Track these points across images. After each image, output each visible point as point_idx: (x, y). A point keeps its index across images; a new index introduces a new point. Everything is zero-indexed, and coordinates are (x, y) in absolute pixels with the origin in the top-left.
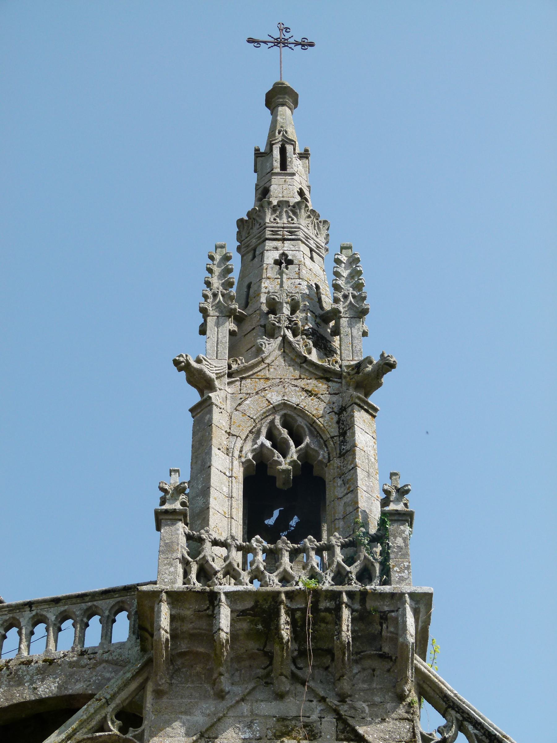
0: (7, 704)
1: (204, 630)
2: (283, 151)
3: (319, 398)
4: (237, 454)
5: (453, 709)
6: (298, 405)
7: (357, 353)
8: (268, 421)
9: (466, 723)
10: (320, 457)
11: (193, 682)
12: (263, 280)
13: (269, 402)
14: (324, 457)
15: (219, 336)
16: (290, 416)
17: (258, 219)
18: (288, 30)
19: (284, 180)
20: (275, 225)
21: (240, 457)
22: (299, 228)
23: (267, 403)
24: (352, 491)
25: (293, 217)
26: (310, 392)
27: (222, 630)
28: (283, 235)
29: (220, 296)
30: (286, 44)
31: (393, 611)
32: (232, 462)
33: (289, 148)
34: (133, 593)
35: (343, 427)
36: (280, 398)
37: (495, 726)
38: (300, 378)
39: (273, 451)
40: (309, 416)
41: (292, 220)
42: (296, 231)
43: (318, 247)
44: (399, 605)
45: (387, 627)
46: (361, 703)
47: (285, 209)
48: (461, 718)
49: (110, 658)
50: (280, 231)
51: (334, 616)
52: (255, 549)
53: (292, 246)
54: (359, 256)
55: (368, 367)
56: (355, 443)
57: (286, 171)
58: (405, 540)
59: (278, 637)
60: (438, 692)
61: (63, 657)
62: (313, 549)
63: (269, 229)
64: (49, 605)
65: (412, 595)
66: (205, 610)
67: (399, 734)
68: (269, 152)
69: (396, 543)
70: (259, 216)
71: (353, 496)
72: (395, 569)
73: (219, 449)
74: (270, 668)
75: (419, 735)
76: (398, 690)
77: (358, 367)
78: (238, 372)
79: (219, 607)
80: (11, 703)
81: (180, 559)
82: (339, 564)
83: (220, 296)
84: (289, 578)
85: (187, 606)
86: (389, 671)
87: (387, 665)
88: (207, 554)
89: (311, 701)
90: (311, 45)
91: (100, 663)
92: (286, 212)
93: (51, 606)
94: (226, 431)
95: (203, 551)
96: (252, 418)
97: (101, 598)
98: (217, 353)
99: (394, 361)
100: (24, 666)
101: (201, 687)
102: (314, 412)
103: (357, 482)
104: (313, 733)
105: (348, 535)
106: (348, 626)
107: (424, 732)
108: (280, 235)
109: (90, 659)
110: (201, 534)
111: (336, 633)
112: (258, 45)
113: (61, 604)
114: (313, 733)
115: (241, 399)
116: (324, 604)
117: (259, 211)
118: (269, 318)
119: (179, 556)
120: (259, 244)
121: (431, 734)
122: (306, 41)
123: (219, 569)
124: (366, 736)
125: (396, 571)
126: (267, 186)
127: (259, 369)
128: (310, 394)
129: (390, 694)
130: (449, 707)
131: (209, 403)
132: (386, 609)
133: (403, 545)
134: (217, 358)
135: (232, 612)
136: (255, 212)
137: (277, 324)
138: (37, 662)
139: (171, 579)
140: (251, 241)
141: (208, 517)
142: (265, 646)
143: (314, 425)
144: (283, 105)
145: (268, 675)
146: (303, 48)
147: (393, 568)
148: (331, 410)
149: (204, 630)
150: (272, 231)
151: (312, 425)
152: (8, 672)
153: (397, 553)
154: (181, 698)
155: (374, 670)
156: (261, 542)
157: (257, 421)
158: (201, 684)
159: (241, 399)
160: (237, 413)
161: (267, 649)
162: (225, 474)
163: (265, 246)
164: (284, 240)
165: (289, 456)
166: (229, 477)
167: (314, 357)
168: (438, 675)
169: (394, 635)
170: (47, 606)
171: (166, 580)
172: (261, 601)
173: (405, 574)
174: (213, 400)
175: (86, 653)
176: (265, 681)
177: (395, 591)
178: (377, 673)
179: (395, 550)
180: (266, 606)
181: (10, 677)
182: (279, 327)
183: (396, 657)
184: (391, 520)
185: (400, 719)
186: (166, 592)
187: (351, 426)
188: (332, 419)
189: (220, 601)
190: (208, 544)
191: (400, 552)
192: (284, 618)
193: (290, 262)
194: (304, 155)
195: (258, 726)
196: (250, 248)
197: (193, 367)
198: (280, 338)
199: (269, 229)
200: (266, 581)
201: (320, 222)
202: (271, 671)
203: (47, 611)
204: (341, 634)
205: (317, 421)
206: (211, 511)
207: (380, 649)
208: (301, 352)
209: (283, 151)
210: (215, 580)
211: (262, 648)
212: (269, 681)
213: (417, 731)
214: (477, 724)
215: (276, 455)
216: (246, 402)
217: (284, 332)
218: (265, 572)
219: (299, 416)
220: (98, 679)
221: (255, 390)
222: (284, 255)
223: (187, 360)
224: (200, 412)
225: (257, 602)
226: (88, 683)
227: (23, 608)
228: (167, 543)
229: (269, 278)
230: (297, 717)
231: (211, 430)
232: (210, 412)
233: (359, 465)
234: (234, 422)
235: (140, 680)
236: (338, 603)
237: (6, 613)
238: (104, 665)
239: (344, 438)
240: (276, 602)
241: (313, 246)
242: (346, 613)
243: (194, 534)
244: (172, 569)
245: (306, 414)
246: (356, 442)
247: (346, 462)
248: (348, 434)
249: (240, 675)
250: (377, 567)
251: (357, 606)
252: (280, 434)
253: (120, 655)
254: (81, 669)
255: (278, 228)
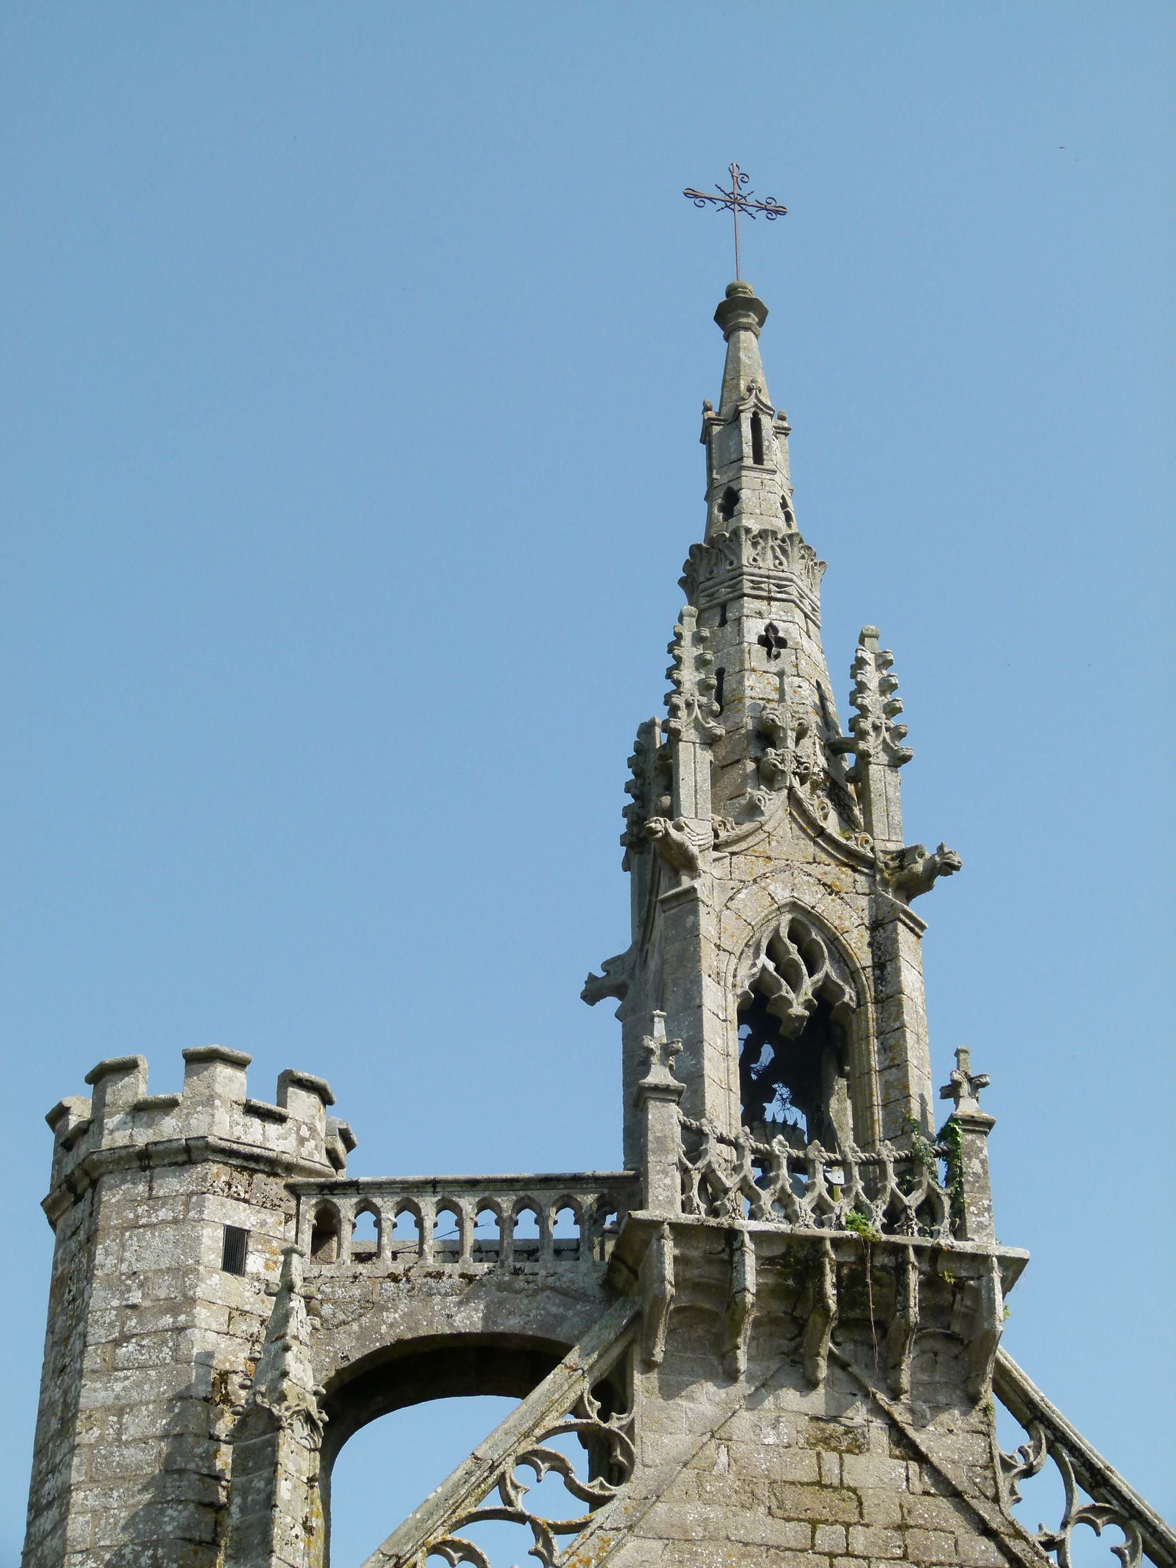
0: (410, 1336)
1: (714, 1279)
2: (756, 424)
3: (842, 899)
4: (730, 980)
5: (1042, 1422)
6: (813, 908)
7: (895, 828)
8: (771, 929)
9: (1059, 1446)
10: (846, 998)
11: (693, 1351)
12: (747, 674)
13: (772, 898)
14: (851, 998)
15: (698, 779)
16: (803, 924)
17: (727, 552)
18: (746, 179)
19: (760, 480)
20: (756, 571)
21: (734, 986)
22: (791, 580)
23: (770, 899)
24: (899, 1065)
25: (781, 557)
26: (829, 887)
27: (749, 1291)
28: (770, 591)
29: (697, 709)
30: (744, 207)
31: (972, 1279)
32: (726, 997)
33: (767, 423)
34: (585, 1186)
35: (879, 953)
36: (787, 894)
37: (1096, 1451)
38: (815, 862)
39: (779, 981)
40: (829, 928)
41: (781, 564)
42: (786, 586)
43: (814, 610)
44: (982, 1271)
45: (962, 1300)
46: (921, 1403)
47: (769, 545)
48: (1052, 1438)
49: (558, 1284)
50: (765, 582)
51: (894, 1278)
52: (778, 1157)
53: (783, 613)
54: (892, 657)
55: (916, 862)
56: (900, 988)
57: (762, 464)
58: (983, 1162)
59: (823, 1307)
60: (1021, 1394)
61: (489, 1274)
62: (856, 1163)
63: (749, 577)
64: (462, 1187)
65: (1001, 1259)
66: (719, 1253)
67: (972, 1454)
68: (730, 420)
69: (972, 1169)
70: (729, 547)
71: (900, 1074)
72: (972, 1209)
73: (710, 976)
74: (798, 1339)
75: (998, 1458)
76: (971, 1389)
77: (902, 855)
78: (727, 844)
79: (743, 1255)
80: (416, 1335)
81: (676, 1164)
82: (892, 1190)
83: (697, 709)
84: (825, 1207)
85: (695, 1243)
86: (956, 1357)
87: (956, 1349)
88: (713, 1159)
89: (855, 1395)
90: (780, 211)
91: (543, 1290)
92: (772, 548)
93: (464, 1189)
94: (715, 944)
95: (707, 1154)
96: (750, 924)
97: (538, 1187)
98: (696, 808)
99: (959, 862)
100: (432, 1280)
101: (705, 1359)
102: (837, 923)
103: (906, 1054)
104: (858, 1443)
105: (892, 1135)
106: (915, 1298)
107: (1004, 1453)
108: (765, 590)
109: (528, 1283)
110: (701, 1125)
111: (899, 1307)
112: (702, 204)
113: (478, 1187)
114: (858, 1443)
115: (733, 889)
116: (883, 1260)
117: (730, 539)
118: (767, 753)
119: (676, 1160)
120: (732, 599)
121: (1011, 1457)
122: (774, 203)
123: (732, 1186)
124: (930, 1455)
125: (973, 1213)
126: (736, 488)
127: (757, 840)
128: (829, 890)
129: (958, 1392)
130: (1036, 1418)
131: (692, 897)
132: (964, 1274)
133: (980, 1171)
134: (696, 817)
135: (757, 1258)
136: (723, 539)
137: (780, 766)
138: (450, 1276)
139: (668, 1197)
140: (717, 588)
141: (703, 1090)
142: (794, 1309)
143: (836, 943)
144: (747, 328)
145: (796, 1350)
146: (769, 216)
147: (968, 1208)
148: (860, 922)
149: (714, 1279)
150: (752, 581)
151: (832, 943)
152: (408, 1286)
153: (973, 1184)
154: (680, 1374)
155: (936, 1354)
156: (784, 1146)
157: (756, 928)
158: (705, 1354)
159: (733, 889)
160: (727, 912)
161: (797, 1313)
162: (717, 1016)
163: (742, 607)
164: (770, 599)
165: (803, 991)
166: (724, 1021)
167: (832, 825)
168: (1018, 1367)
169: (971, 1312)
170: (459, 1189)
171: (661, 1198)
172: (795, 1247)
173: (985, 1219)
174: (700, 895)
175: (522, 1272)
176: (791, 1358)
177: (979, 1252)
178: (940, 1359)
179: (970, 1178)
180: (801, 1255)
181: (411, 1294)
182: (783, 772)
183: (970, 1342)
184: (964, 1130)
185: (973, 1432)
186: (669, 1224)
187: (893, 955)
188: (862, 936)
189: (743, 1243)
190: (712, 1141)
191: (978, 1182)
192: (830, 1278)
193: (782, 643)
194: (782, 431)
195: (786, 1426)
196: (716, 601)
197: (674, 841)
198: (786, 791)
199: (749, 577)
200: (796, 1211)
201: (816, 564)
202: (800, 1345)
203: (459, 1197)
204: (908, 1311)
205: (841, 938)
206: (707, 1081)
207: (948, 1327)
208: (816, 819)
209: (756, 424)
210: (727, 1203)
211: (790, 1311)
212: (797, 1359)
213: (996, 1453)
214: (1075, 1450)
215: (784, 989)
216: (739, 896)
217: (791, 782)
218: (794, 1196)
219: (813, 924)
220: (541, 1315)
221: (752, 875)
222: (771, 628)
223: (665, 829)
224: (676, 907)
225: (789, 1247)
226: (527, 1319)
227: (423, 1187)
228: (658, 1137)
229: (753, 670)
230: (836, 1417)
231: (699, 943)
232: (695, 912)
233: (908, 1025)
234: (725, 928)
235: (624, 1342)
236: (900, 1260)
237: (398, 1190)
238: (548, 1293)
239: (882, 972)
240: (817, 1251)
241: (808, 610)
242: (913, 1278)
243: (691, 1124)
244: (668, 1181)
245: (825, 925)
246: (903, 986)
247: (886, 1015)
248: (889, 969)
249: (758, 1345)
250: (947, 1203)
251: (926, 1267)
252: (788, 952)
253: (572, 1282)
254: (514, 1295)
255: (761, 576)
